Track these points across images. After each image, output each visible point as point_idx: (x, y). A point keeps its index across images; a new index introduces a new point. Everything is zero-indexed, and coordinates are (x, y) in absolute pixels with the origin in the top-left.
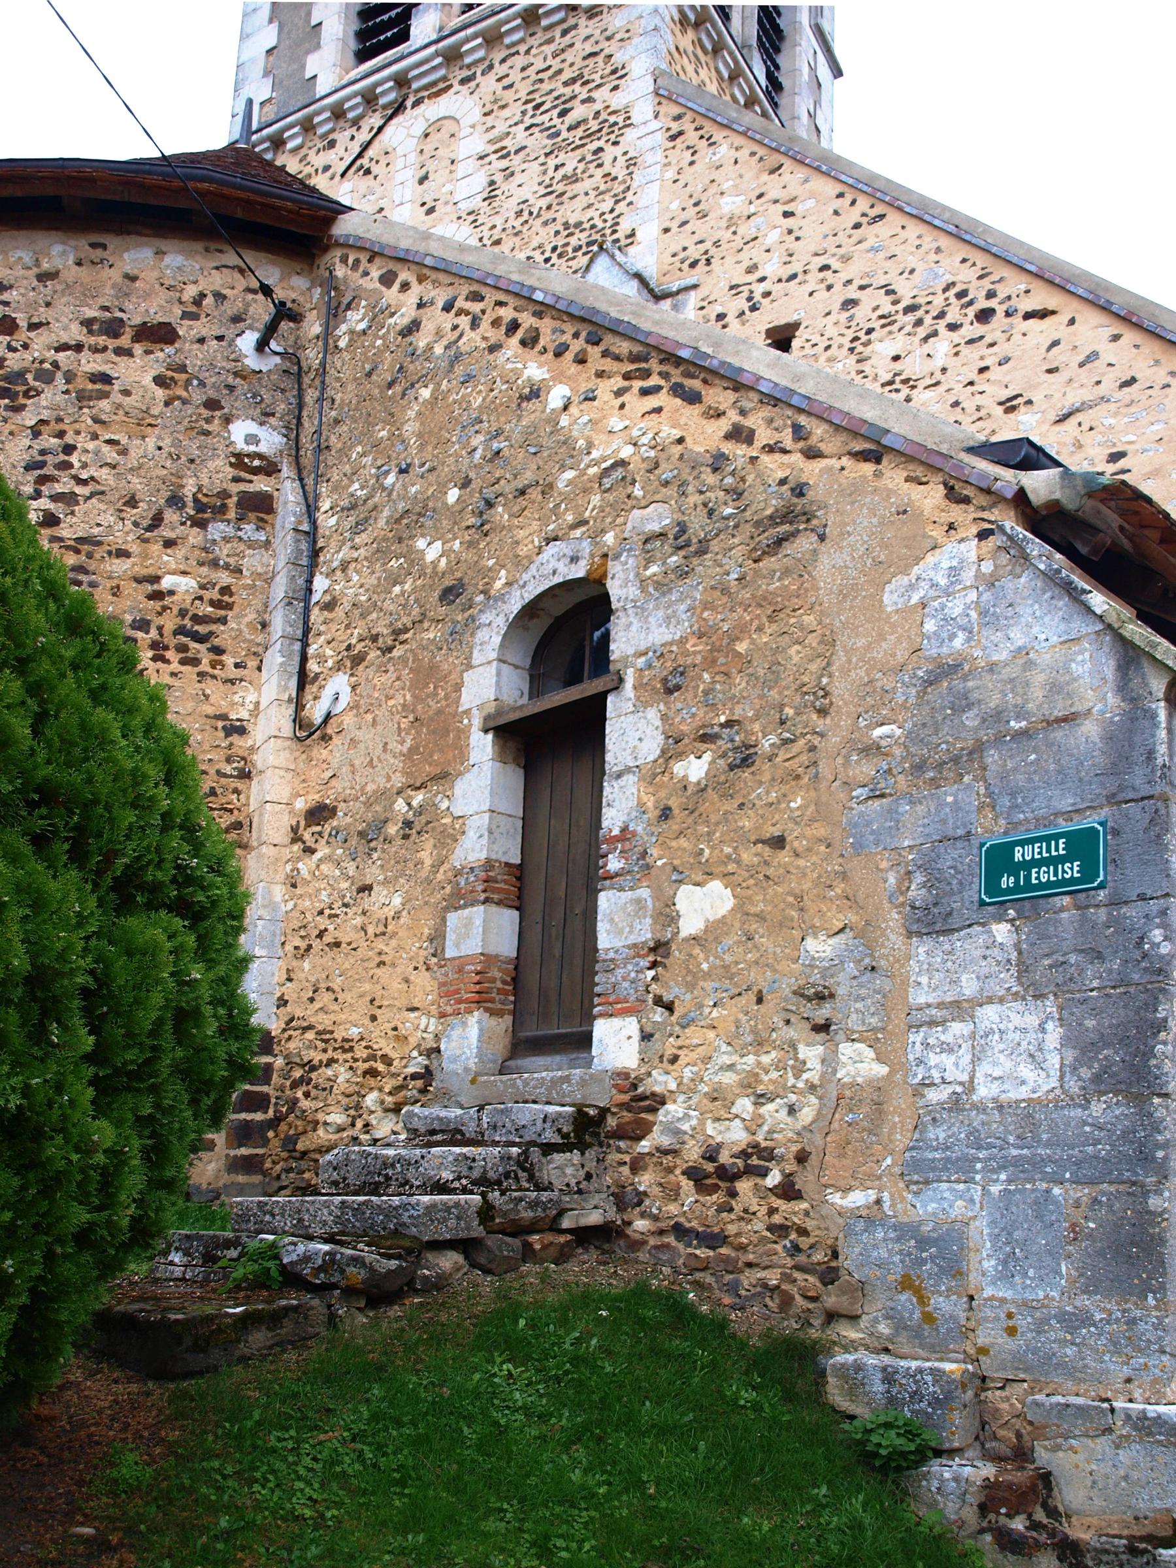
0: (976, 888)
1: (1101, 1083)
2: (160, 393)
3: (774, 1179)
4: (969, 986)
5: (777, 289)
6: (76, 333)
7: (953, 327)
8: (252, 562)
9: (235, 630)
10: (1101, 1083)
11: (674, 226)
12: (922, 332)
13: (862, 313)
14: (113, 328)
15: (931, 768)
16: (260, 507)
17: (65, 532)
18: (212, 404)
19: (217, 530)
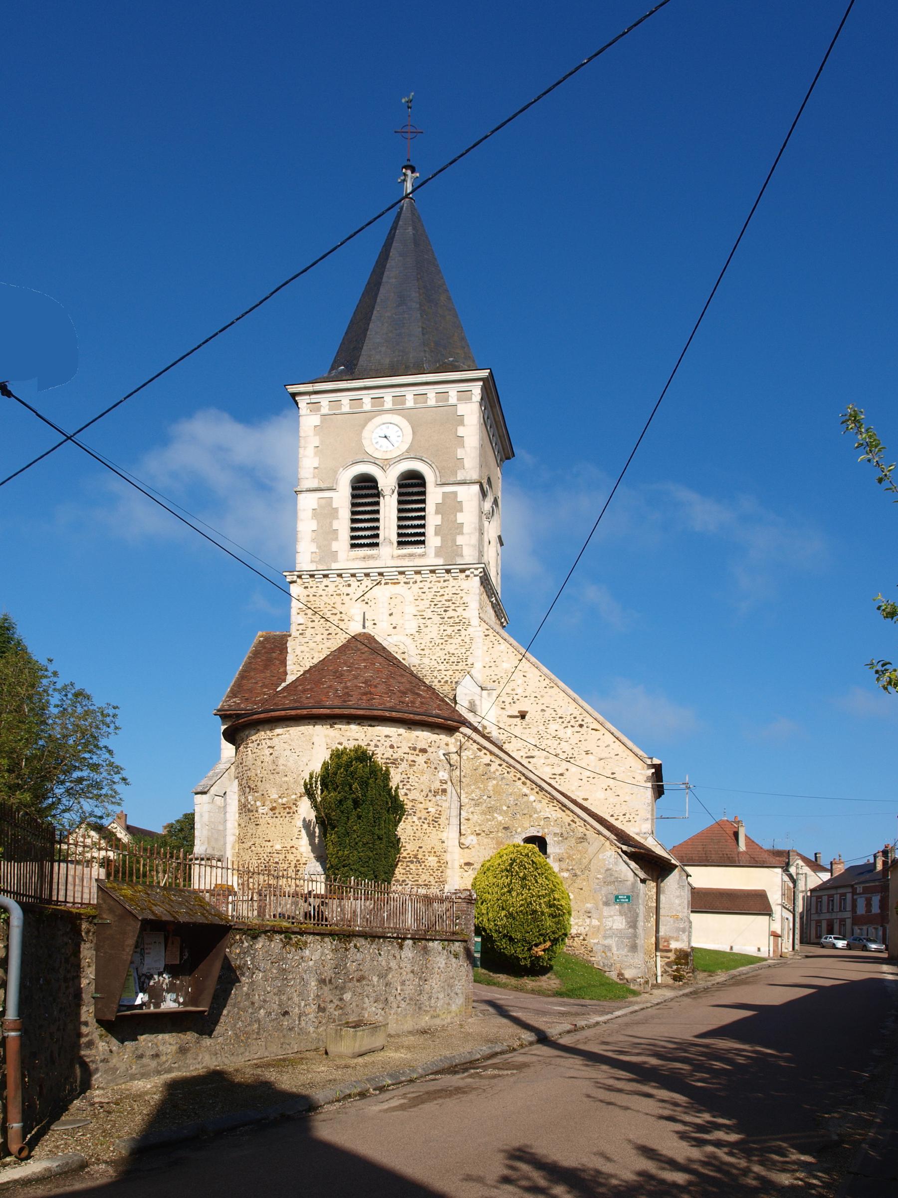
0: (614, 900)
1: (630, 927)
2: (426, 765)
3: (581, 938)
4: (612, 913)
5: (521, 699)
6: (407, 750)
7: (572, 726)
8: (445, 805)
9: (442, 821)
10: (630, 927)
11: (487, 666)
12: (564, 725)
13: (547, 714)
14: (415, 749)
15: (606, 883)
16: (444, 791)
17: (409, 797)
18: (436, 768)
19: (438, 797)
